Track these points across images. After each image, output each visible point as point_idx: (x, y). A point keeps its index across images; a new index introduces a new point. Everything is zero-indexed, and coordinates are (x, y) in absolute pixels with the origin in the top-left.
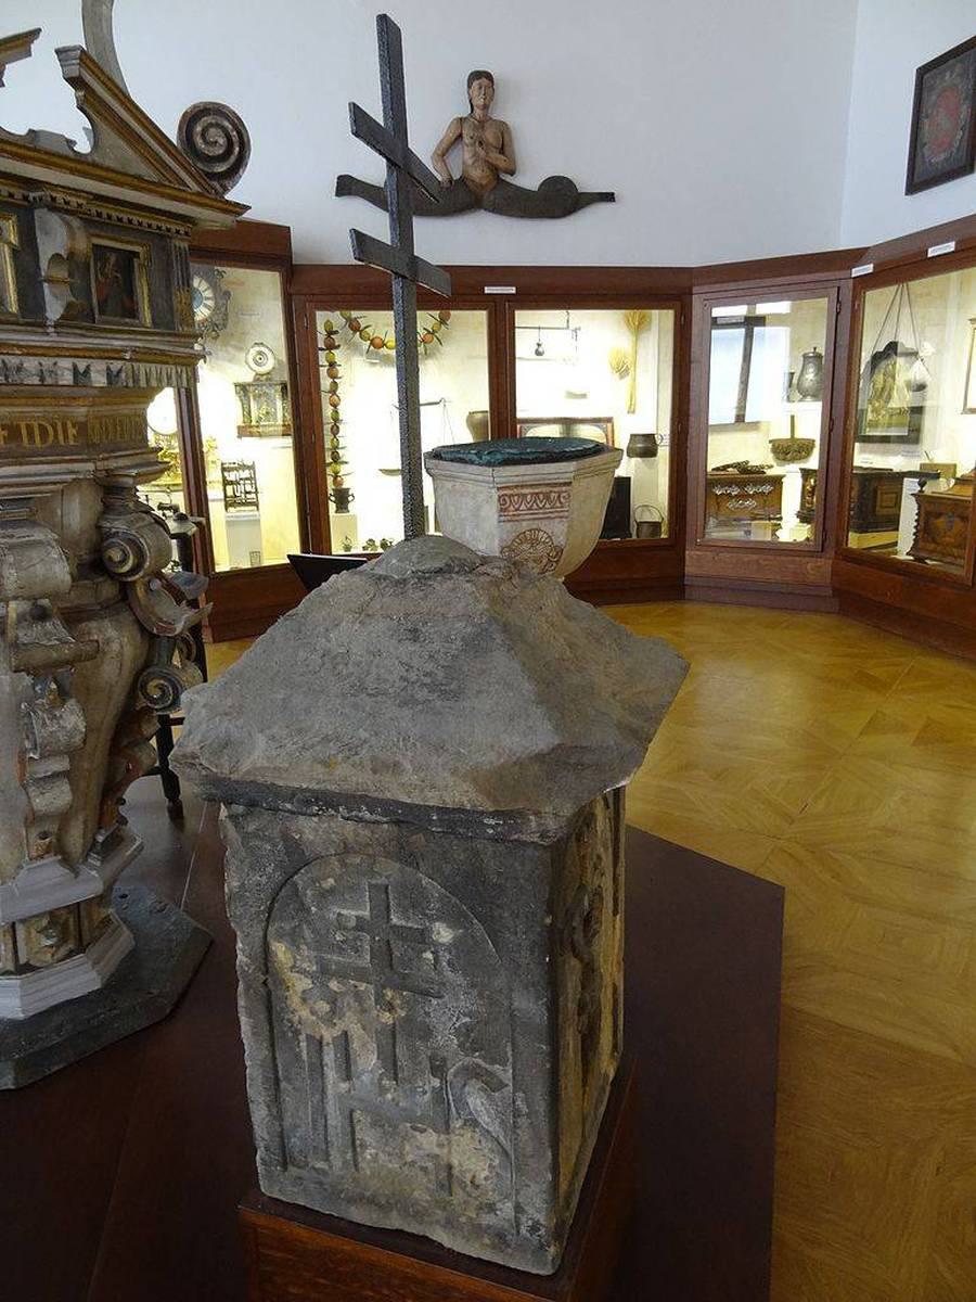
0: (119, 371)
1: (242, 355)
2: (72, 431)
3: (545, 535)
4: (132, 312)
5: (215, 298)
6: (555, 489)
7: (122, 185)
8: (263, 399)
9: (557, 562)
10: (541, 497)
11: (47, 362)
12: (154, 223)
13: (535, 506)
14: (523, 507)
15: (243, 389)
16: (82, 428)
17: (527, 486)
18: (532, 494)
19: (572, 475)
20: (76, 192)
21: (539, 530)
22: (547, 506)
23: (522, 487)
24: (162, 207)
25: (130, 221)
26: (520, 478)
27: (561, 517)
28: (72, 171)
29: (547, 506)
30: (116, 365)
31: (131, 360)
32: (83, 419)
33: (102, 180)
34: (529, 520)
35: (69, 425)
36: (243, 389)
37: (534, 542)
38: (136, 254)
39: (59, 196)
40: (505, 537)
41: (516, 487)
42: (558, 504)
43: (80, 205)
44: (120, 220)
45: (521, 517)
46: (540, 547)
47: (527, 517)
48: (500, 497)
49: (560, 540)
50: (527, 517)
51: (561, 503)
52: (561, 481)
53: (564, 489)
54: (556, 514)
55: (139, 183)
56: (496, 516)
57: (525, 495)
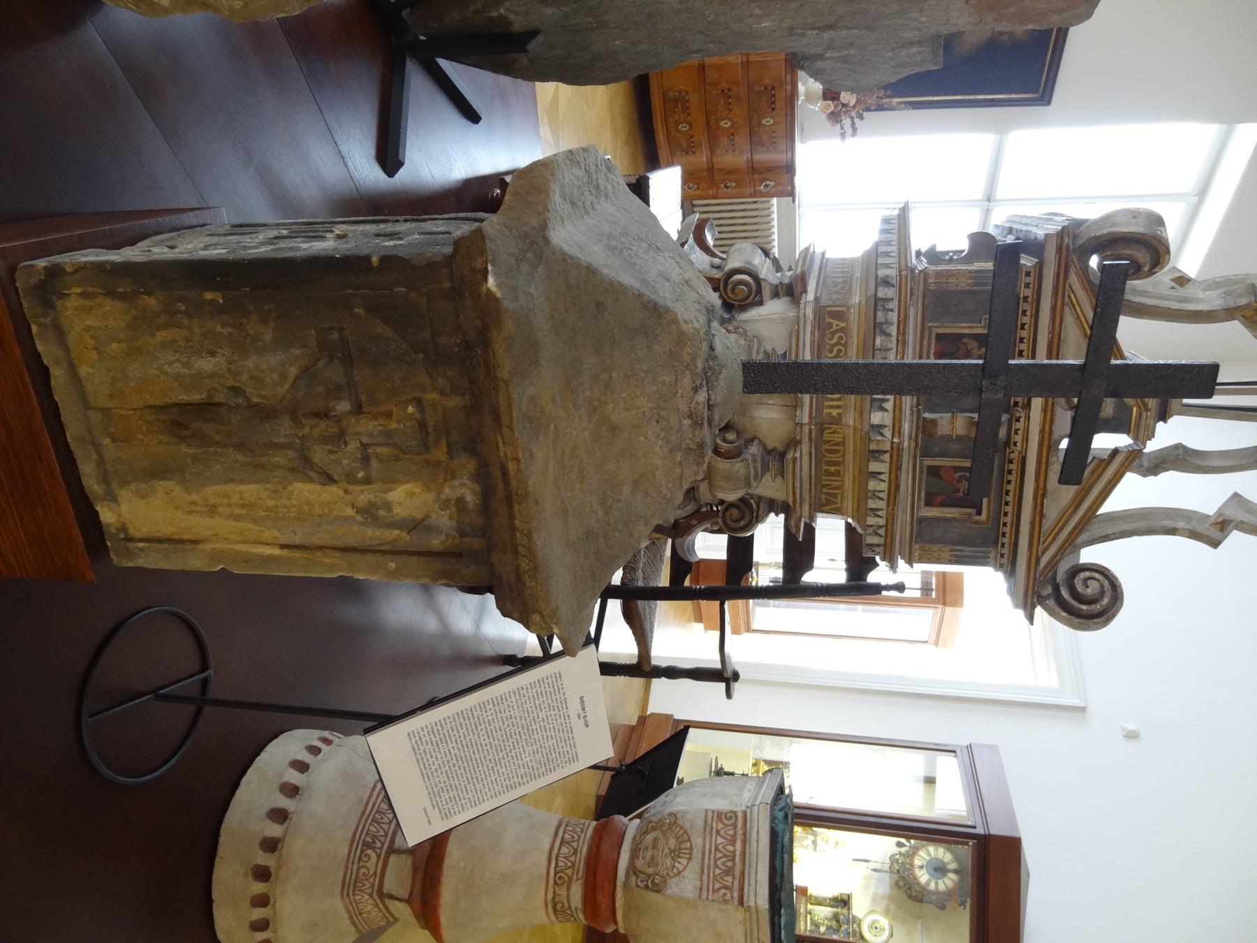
0: (882, 435)
1: (881, 909)
2: (835, 412)
3: (681, 868)
4: (929, 503)
5: (937, 893)
6: (736, 882)
7: (1037, 481)
8: (834, 923)
9: (647, 887)
10: (729, 864)
11: (893, 330)
12: (1007, 530)
13: (719, 855)
14: (720, 840)
15: (843, 902)
16: (838, 421)
17: (744, 847)
18: (734, 852)
19: (752, 904)
20: (1026, 439)
21: (689, 859)
22: (718, 871)
23: (744, 842)
24: (1023, 516)
25: (1009, 482)
26: (754, 837)
27: (701, 889)
28: (1042, 432)
29: (718, 871)
30: (888, 433)
31: (893, 443)
32: (844, 421)
33: (1039, 462)
34: (704, 847)
35: (840, 411)
36: (843, 902)
37: (675, 854)
38: (979, 513)
39: (1020, 425)
40: (688, 816)
41: (745, 834)
42: (717, 886)
43: (1015, 444)
44: (1007, 493)
45: (708, 838)
46: (668, 862)
47: (708, 844)
48: (735, 813)
49: (673, 888)
50: (708, 844)
51: (718, 890)
52: (746, 890)
53: (736, 895)
54: (705, 882)
55: (1039, 512)
56: (714, 808)
57: (733, 843)
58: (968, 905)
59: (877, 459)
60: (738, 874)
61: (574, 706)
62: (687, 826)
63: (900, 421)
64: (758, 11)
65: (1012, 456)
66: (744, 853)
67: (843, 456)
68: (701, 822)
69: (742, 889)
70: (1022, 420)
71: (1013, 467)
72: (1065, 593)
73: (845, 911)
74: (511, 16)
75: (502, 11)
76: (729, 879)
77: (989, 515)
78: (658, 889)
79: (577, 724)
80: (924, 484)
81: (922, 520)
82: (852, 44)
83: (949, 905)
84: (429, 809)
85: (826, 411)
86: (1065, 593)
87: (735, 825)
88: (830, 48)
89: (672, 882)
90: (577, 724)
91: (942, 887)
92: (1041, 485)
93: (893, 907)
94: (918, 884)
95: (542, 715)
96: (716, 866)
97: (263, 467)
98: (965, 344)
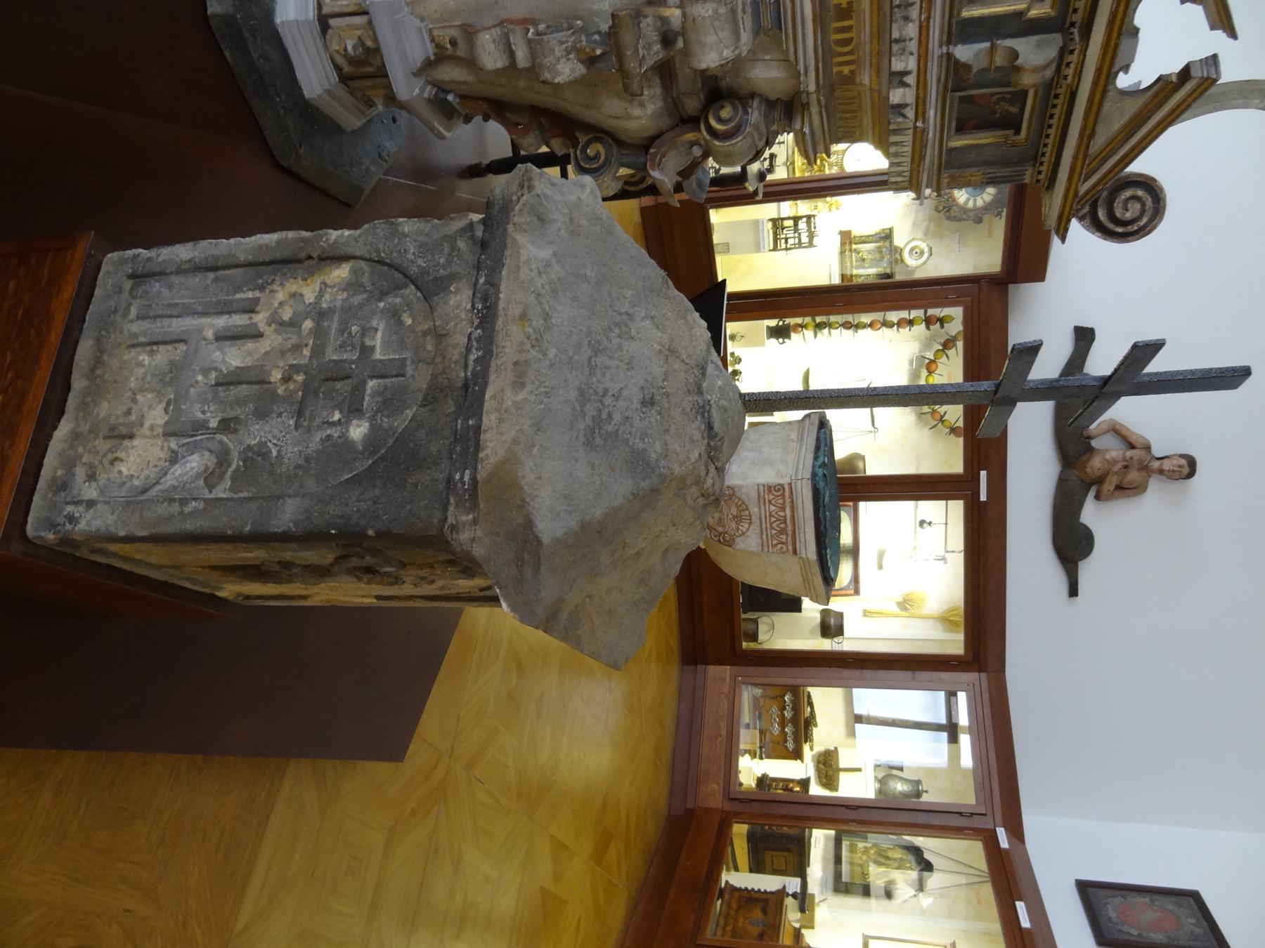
0: (904, 116)
1: (920, 235)
2: (846, 70)
7: (1086, 118)
9: (719, 541)
12: (1048, 150)
14: (772, 508)
16: (850, 80)
19: (803, 555)
20: (1079, 74)
21: (750, 524)
23: (793, 508)
26: (800, 506)
30: (910, 113)
31: (915, 127)
32: (858, 80)
35: (853, 67)
37: (738, 519)
38: (1018, 132)
39: (1074, 58)
40: (744, 490)
44: (1052, 116)
46: (734, 525)
48: (782, 485)
49: (741, 544)
55: (1088, 134)
57: (783, 509)
58: (1004, 214)
60: (790, 533)
62: (744, 498)
63: (924, 102)
65: (1059, 91)
66: (793, 517)
68: (755, 495)
69: (794, 544)
70: (1076, 52)
72: (1102, 214)
73: (887, 244)
76: (784, 537)
77: (1028, 134)
78: (730, 543)
80: (956, 108)
81: (951, 150)
83: (986, 218)
85: (835, 70)
86: (1102, 214)
87: (783, 495)
89: (739, 540)
91: (980, 203)
92: (1090, 125)
93: (932, 226)
94: (957, 205)
96: (772, 528)
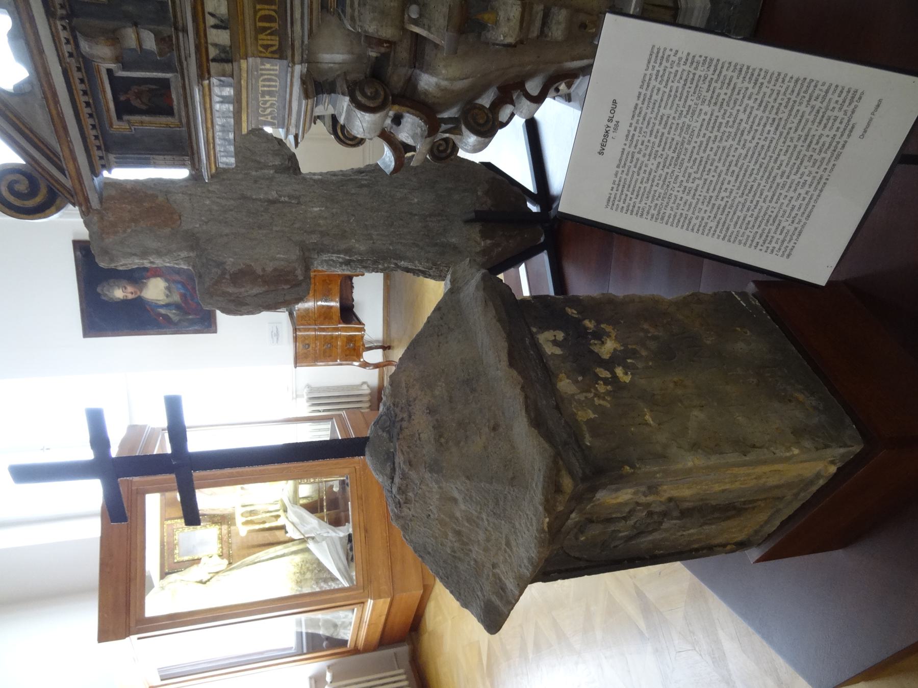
39: (67, 49)
59: (222, 49)
61: (615, 146)
64: (321, 222)
67: (256, 12)
71: (81, 87)
74: (478, 239)
75: (483, 244)
79: (624, 115)
82: (256, 182)
84: (858, 131)
88: (271, 179)
90: (624, 115)
95: (652, 164)
97: (702, 500)
98: (143, 103)
